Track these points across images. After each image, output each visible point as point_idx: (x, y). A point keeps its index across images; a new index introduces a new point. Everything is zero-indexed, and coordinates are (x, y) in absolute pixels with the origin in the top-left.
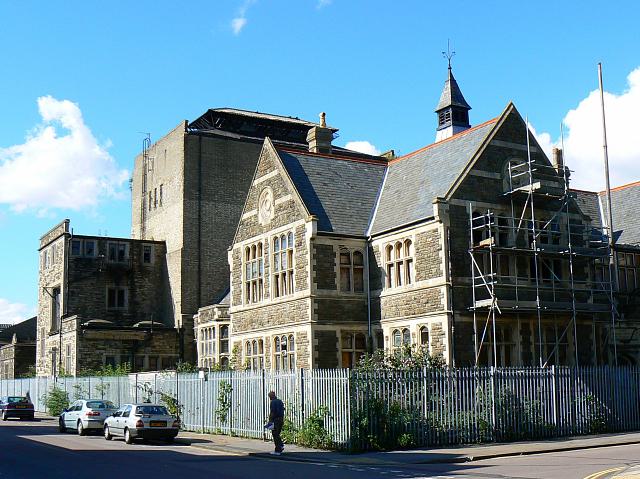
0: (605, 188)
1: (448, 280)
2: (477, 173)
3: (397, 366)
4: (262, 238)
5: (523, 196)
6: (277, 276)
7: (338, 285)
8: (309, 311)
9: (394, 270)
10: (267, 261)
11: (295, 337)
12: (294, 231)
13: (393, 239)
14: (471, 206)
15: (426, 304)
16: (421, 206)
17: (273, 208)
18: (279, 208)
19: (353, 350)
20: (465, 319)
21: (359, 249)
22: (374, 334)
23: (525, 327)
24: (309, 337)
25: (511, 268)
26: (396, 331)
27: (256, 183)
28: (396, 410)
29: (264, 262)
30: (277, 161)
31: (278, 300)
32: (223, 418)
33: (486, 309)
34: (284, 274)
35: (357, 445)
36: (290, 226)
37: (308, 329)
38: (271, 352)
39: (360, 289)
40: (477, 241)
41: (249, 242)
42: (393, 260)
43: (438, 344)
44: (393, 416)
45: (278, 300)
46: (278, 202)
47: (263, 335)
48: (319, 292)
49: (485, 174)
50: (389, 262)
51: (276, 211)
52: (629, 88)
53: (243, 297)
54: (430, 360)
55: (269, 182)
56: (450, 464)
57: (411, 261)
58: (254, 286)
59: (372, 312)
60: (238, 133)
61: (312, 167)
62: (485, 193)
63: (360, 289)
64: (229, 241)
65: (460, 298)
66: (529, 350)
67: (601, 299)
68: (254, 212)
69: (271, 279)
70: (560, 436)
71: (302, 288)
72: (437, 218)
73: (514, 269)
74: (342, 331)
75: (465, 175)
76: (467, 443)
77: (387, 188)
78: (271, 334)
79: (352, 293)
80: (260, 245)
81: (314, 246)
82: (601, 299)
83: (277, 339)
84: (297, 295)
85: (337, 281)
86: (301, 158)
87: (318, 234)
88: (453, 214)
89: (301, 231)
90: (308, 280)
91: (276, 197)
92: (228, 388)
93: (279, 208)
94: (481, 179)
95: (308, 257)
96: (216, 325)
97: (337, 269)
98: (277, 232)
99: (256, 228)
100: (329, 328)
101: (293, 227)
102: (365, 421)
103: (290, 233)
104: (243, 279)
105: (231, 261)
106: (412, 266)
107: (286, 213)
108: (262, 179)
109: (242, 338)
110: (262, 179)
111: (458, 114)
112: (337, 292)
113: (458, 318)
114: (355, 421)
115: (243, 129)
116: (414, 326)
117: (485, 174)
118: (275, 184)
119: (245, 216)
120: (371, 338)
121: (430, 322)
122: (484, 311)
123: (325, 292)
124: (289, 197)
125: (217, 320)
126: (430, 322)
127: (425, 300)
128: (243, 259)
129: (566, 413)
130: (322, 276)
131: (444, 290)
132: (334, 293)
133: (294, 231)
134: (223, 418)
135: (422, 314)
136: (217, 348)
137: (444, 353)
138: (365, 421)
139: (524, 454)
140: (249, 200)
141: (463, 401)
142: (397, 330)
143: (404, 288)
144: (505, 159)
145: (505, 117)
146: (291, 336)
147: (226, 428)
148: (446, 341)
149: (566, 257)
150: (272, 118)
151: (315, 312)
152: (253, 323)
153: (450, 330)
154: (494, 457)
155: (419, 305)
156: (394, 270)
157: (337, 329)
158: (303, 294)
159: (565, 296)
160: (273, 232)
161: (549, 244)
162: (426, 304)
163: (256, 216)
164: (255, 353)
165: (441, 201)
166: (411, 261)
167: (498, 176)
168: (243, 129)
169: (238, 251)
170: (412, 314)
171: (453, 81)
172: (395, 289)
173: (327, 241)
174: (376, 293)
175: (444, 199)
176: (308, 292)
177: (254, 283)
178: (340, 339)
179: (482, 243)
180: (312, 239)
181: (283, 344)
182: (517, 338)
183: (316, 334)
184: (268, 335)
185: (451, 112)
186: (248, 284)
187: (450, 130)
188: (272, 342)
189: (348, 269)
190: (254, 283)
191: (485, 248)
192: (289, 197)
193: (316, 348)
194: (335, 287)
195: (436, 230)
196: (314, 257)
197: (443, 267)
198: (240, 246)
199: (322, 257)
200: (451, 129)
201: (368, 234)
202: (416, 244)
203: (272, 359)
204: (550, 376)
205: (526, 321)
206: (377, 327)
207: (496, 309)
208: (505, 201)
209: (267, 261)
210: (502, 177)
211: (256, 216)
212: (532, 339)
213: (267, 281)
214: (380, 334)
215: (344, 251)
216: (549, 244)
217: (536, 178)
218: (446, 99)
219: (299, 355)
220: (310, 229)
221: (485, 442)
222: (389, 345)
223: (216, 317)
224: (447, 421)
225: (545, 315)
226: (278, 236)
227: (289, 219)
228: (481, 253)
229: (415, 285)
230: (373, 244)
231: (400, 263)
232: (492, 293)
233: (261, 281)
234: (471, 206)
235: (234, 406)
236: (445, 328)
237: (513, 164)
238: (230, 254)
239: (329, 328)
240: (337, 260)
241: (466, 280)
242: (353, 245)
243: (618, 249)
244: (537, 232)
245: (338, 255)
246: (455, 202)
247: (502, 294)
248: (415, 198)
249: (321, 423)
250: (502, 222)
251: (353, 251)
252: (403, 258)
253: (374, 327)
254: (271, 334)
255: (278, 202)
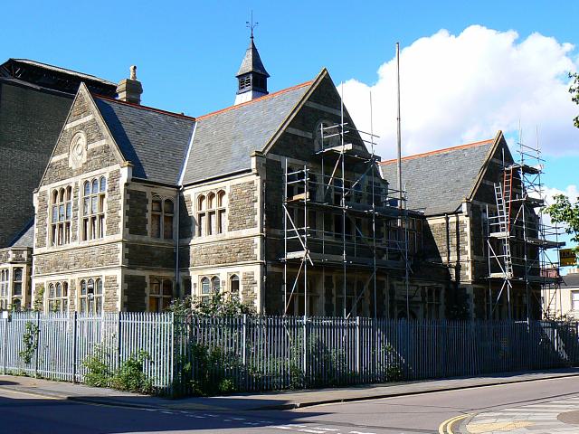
0: (397, 157)
1: (262, 231)
2: (292, 131)
3: (207, 312)
4: (71, 181)
5: (335, 155)
6: (86, 220)
7: (149, 232)
8: (120, 256)
9: (205, 220)
10: (76, 205)
11: (103, 280)
12: (107, 176)
13: (206, 189)
14: (286, 162)
15: (242, 253)
16: (233, 160)
17: (85, 153)
18: (92, 153)
19: (161, 295)
20: (276, 270)
21: (172, 198)
22: (181, 281)
23: (328, 279)
24: (119, 281)
25: (318, 223)
26: (204, 279)
27: (68, 127)
28: (216, 355)
29: (72, 205)
30: (93, 106)
31: (86, 243)
32: (28, 361)
33: (299, 260)
34: (94, 219)
35: (179, 390)
36: (103, 170)
37: (118, 274)
38: (76, 295)
39: (169, 236)
40: (290, 195)
41: (58, 185)
42: (205, 209)
43: (249, 293)
44: (213, 361)
45: (86, 243)
46: (91, 146)
47: (69, 278)
48: (131, 237)
49: (299, 133)
50: (210, 210)
51: (89, 156)
52: (377, 80)
53: (48, 240)
54: (241, 307)
55: (82, 127)
56: (282, 414)
57: (224, 211)
58: (61, 229)
59: (181, 259)
60: (37, 84)
61: (125, 115)
62: (298, 150)
63: (169, 236)
64: (35, 183)
65: (272, 248)
66: (331, 300)
67: (396, 256)
68: (64, 156)
69: (80, 223)
70: (363, 383)
71: (112, 231)
72: (255, 171)
73: (321, 222)
74: (151, 277)
75: (281, 132)
76: (280, 389)
77: (196, 141)
78: (77, 277)
79: (162, 241)
80: (70, 189)
81: (127, 191)
82: (396, 256)
83: (83, 282)
84: (107, 239)
85: (148, 227)
86: (115, 107)
87: (133, 180)
88: (269, 169)
89: (115, 177)
90: (121, 225)
91: (89, 141)
92: (34, 330)
93: (92, 153)
94: (295, 136)
95: (121, 202)
96: (10, 267)
97: (148, 216)
98: (89, 176)
99: (65, 171)
100: (138, 273)
101: (106, 172)
102: (188, 366)
103: (102, 178)
104: (48, 221)
105: (36, 203)
106: (225, 217)
107: (103, 157)
108: (74, 124)
109: (45, 281)
110: (74, 124)
111: (257, 80)
112: (148, 238)
113: (270, 268)
114: (178, 367)
115: (42, 81)
116: (224, 274)
117: (299, 133)
118: (91, 132)
119: (54, 159)
120: (178, 285)
121: (241, 271)
122: (295, 263)
123: (137, 237)
124: (104, 142)
125: (11, 263)
126: (241, 271)
127: (237, 250)
128: (50, 202)
129: (368, 361)
130: (134, 223)
131: (258, 240)
132: (145, 239)
133: (107, 176)
134: (28, 361)
135: (234, 262)
136: (10, 290)
137: (255, 301)
138: (188, 366)
139: (345, 400)
140: (59, 144)
141: (275, 351)
142: (205, 278)
143: (215, 236)
144: (317, 121)
145: (320, 81)
146: (98, 280)
147: (31, 370)
148: (257, 290)
149: (370, 216)
150: (70, 73)
151: (126, 256)
152: (57, 266)
153: (262, 279)
154: (416, 430)
155: (226, 256)
156: (205, 220)
157: (147, 274)
158: (113, 238)
159: (366, 252)
160: (85, 176)
161: (352, 201)
162: (242, 253)
163: (66, 160)
164: (58, 295)
165: (258, 155)
166: (224, 211)
167: (310, 136)
168: (42, 81)
169: (44, 194)
170: (223, 263)
171: (254, 50)
172: (205, 238)
173: (140, 188)
174: (185, 241)
175: (262, 153)
176: (120, 236)
177: (61, 226)
178: (148, 285)
179: (295, 198)
180: (126, 184)
181: (90, 288)
182: (321, 290)
183: (126, 279)
184: (73, 278)
185: (251, 78)
186: (54, 227)
187: (250, 94)
188: (77, 284)
189: (159, 216)
190: (61, 226)
191: (300, 203)
192: (104, 142)
193: (125, 292)
194: (146, 233)
195: (252, 183)
196: (127, 202)
197: (257, 218)
198: (47, 189)
199: (135, 201)
200: (250, 93)
201: (180, 184)
202: (230, 195)
203: (77, 302)
204: (355, 327)
205: (329, 274)
206: (185, 274)
207: (308, 261)
208: (316, 160)
209: (76, 205)
210: (314, 136)
211: (66, 160)
212: (334, 291)
213: (75, 224)
214: (188, 282)
215: (156, 199)
216: (352, 201)
217: (346, 142)
218: (247, 65)
219: (107, 300)
220: (125, 174)
221: (298, 388)
222: (196, 292)
223: (10, 260)
224: (265, 365)
225: (350, 269)
226: (90, 180)
227: (102, 164)
228: (296, 208)
229: (227, 234)
230: (185, 193)
231: (211, 213)
232: (304, 246)
233: (68, 224)
234: (286, 162)
235: (41, 346)
236: (257, 278)
237: (325, 126)
238: (36, 196)
239: (138, 273)
240: (149, 207)
241: (278, 232)
242: (166, 193)
243: (402, 212)
244: (346, 191)
245: (150, 202)
246: (271, 156)
247: (314, 247)
248: (227, 152)
249: (140, 367)
250: (312, 177)
251: (164, 199)
252: (215, 207)
253: (182, 274)
254: (77, 277)
255: (91, 146)
